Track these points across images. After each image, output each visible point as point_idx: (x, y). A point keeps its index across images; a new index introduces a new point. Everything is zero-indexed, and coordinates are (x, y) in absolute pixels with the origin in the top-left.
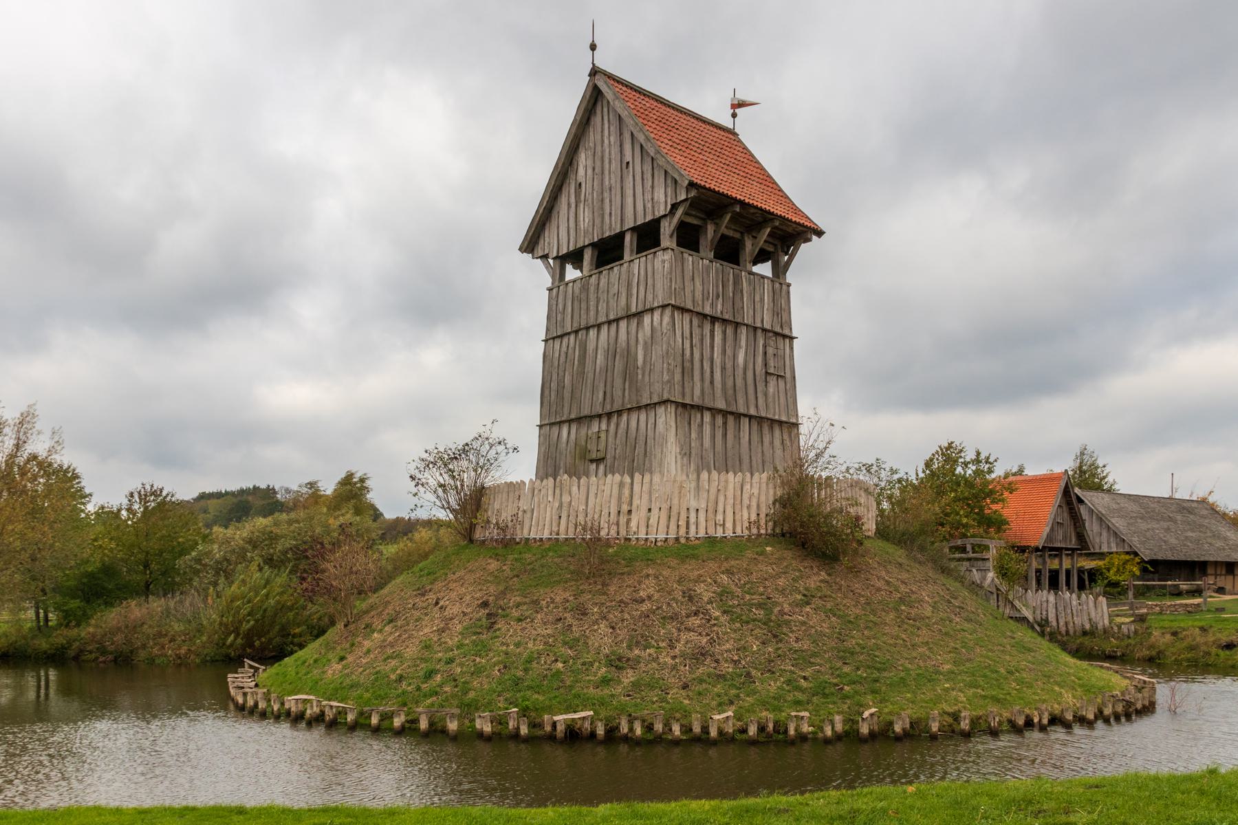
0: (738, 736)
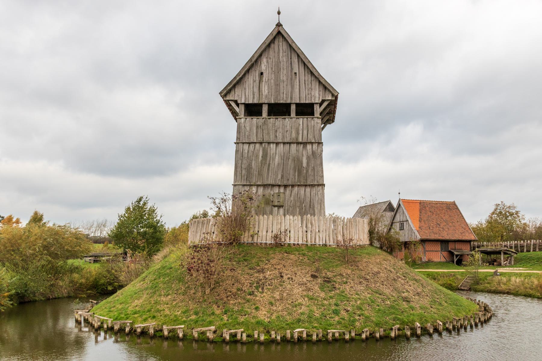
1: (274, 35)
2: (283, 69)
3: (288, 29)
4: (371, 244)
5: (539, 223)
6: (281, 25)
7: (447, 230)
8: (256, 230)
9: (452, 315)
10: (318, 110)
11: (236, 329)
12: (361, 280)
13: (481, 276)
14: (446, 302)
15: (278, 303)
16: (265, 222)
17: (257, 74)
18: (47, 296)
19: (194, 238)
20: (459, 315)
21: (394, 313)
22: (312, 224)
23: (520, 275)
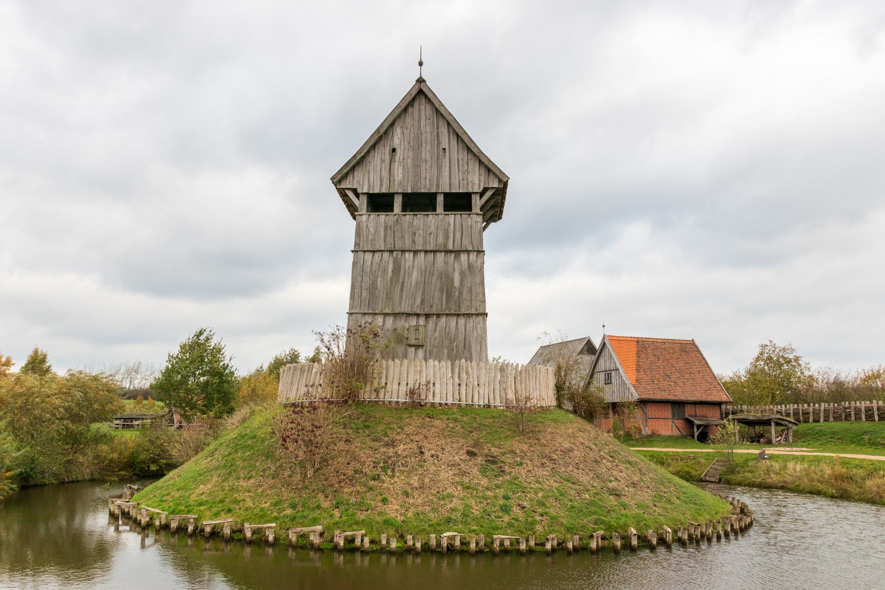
0: (539, 548)
1: (413, 95)
2: (426, 143)
3: (433, 85)
4: (559, 406)
5: (834, 376)
6: (424, 81)
7: (681, 385)
8: (383, 381)
9: (687, 518)
10: (477, 203)
11: (353, 530)
12: (544, 461)
13: (738, 460)
14: (678, 498)
15: (416, 494)
16: (397, 369)
17: (387, 150)
18: (61, 478)
19: (290, 389)
20: (699, 518)
21: (595, 513)
22: (467, 373)
23: (803, 459)
